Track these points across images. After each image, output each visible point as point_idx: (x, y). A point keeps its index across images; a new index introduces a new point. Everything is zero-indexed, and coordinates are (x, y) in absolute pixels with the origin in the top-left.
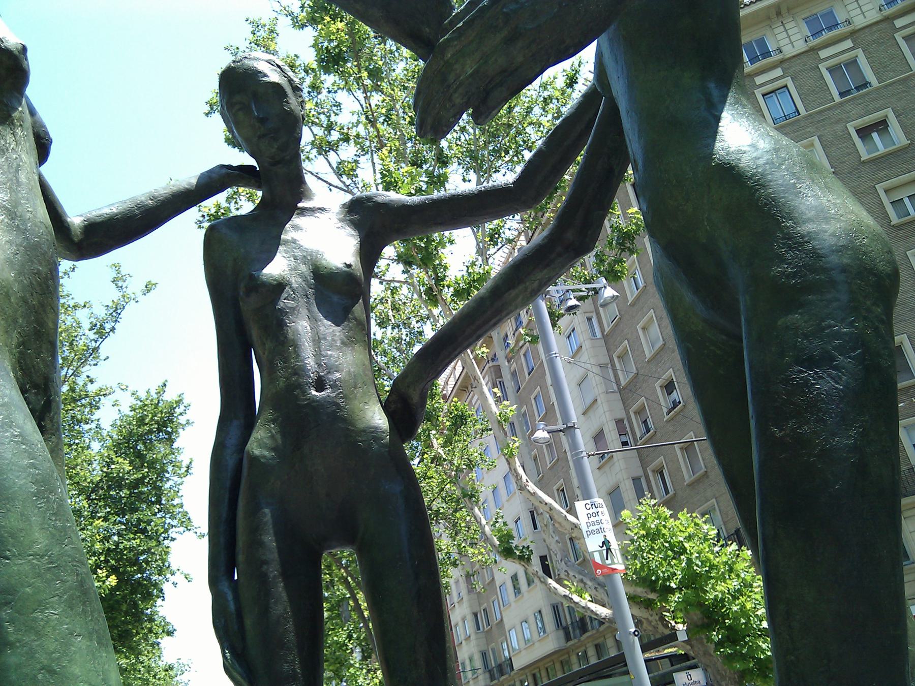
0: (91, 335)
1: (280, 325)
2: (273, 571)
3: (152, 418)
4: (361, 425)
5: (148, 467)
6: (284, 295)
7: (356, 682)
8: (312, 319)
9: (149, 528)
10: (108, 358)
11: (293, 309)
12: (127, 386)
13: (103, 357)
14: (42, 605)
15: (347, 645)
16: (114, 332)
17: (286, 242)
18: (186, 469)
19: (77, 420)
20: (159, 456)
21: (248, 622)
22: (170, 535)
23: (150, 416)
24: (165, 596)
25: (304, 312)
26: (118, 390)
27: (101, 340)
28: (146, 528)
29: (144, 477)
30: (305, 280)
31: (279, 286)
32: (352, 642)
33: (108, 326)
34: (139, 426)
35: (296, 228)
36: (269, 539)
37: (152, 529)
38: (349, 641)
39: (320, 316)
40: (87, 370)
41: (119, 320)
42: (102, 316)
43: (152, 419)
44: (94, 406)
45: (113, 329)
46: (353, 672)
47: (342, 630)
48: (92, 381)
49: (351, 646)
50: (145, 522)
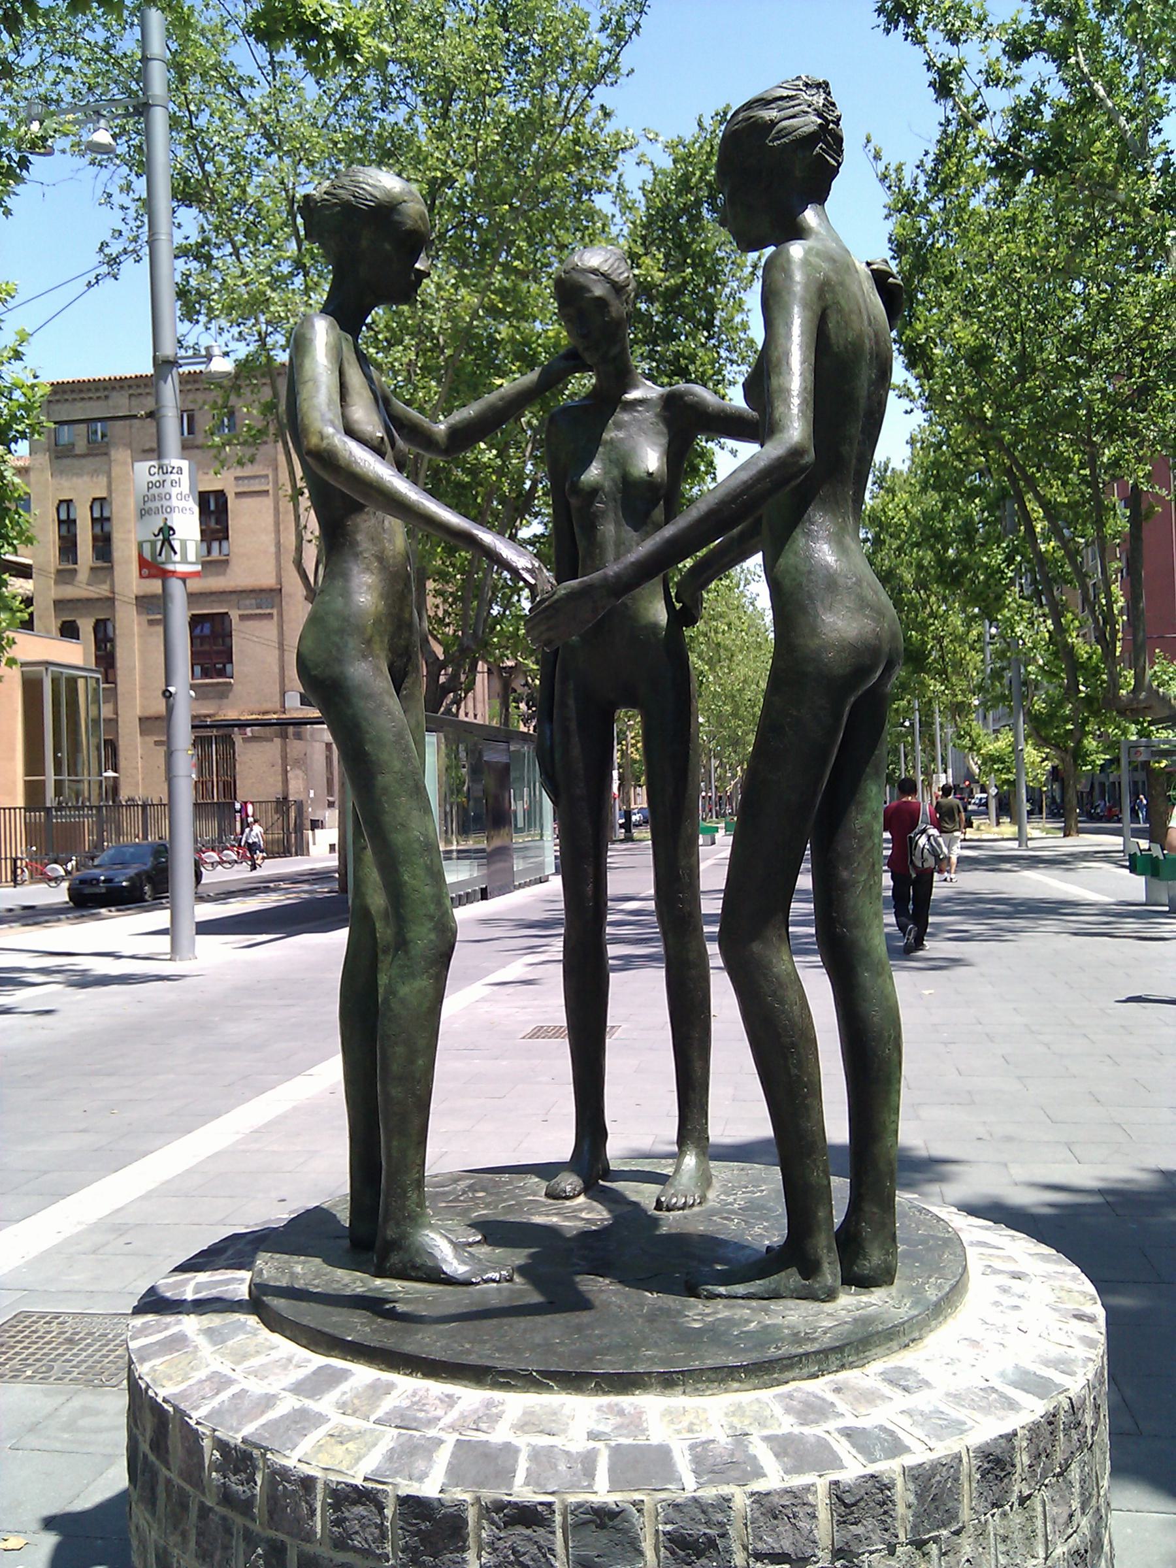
0: (603, 40)
1: (593, 527)
2: (573, 726)
3: (701, 177)
4: (643, 622)
5: (693, 266)
6: (598, 499)
7: (1012, 631)
8: (618, 524)
9: (692, 368)
10: (633, 70)
11: (603, 512)
12: (657, 135)
13: (624, 71)
14: (399, 797)
15: (1003, 572)
16: (638, 34)
17: (606, 442)
18: (750, 269)
19: (586, 186)
20: (710, 247)
21: (557, 756)
22: (728, 376)
23: (698, 173)
24: (717, 472)
25: (611, 515)
26: (643, 141)
27: (618, 49)
28: (687, 366)
29: (685, 283)
30: (616, 484)
31: (594, 491)
32: (1012, 567)
33: (629, 22)
34: (679, 194)
35: (619, 426)
36: (571, 702)
37: (697, 370)
38: (1008, 566)
39: (624, 522)
40: (602, 94)
41: (646, 9)
42: (619, 3)
43: (701, 179)
44: (608, 167)
45: (637, 27)
46: (1008, 615)
47: (998, 547)
48: (607, 115)
49: (1010, 574)
50: (685, 358)
